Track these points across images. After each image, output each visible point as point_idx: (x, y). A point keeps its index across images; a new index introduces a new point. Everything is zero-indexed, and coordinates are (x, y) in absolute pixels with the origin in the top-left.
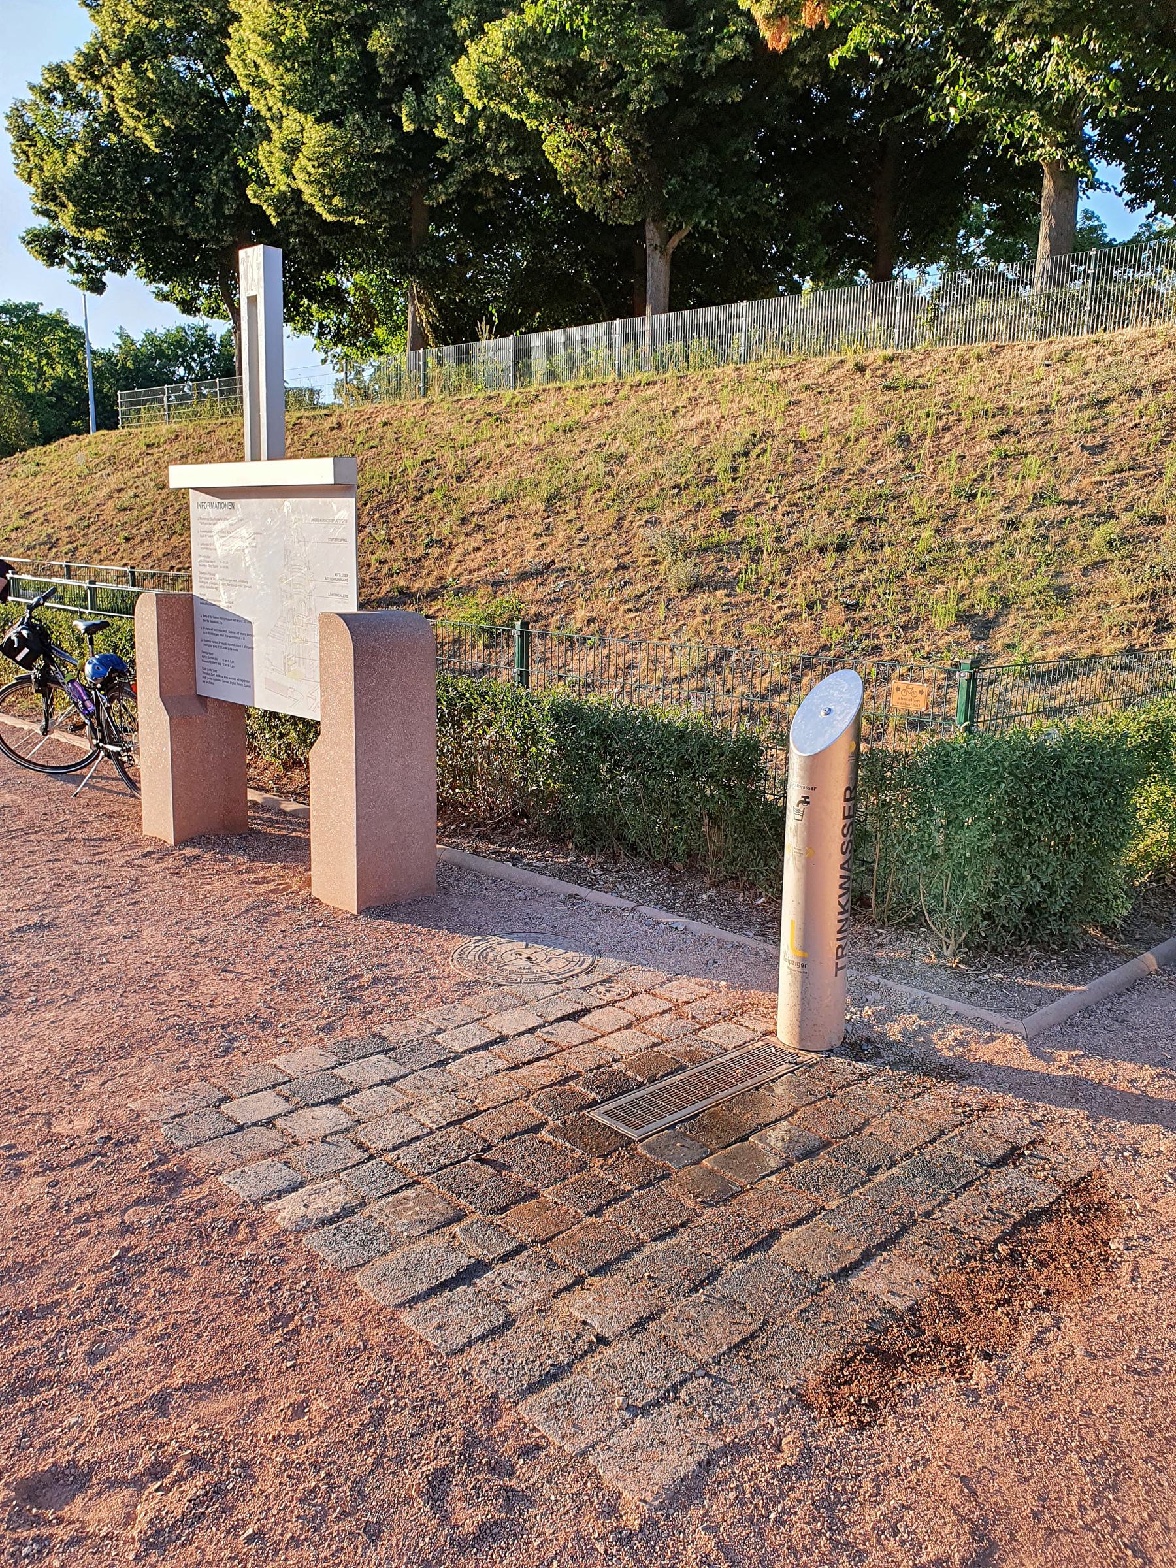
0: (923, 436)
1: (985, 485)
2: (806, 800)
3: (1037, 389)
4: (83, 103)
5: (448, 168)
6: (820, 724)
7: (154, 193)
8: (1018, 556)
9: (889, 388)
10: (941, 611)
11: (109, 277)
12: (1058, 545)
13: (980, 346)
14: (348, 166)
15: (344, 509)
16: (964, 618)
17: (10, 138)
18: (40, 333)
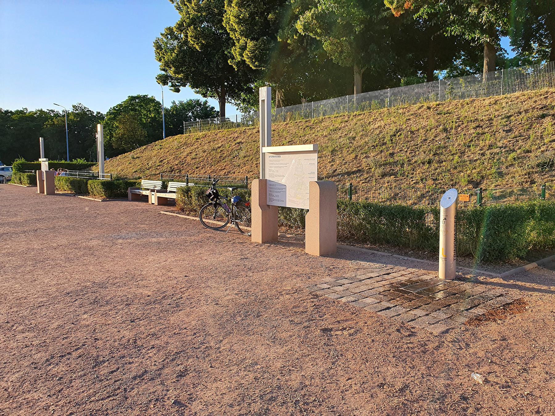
0: (452, 128)
1: (473, 143)
2: (445, 219)
3: (487, 113)
4: (177, 38)
5: (292, 52)
6: (448, 202)
7: (198, 62)
8: (485, 163)
9: (439, 114)
10: (463, 180)
11: (181, 88)
12: (497, 160)
13: (467, 100)
14: (260, 52)
15: (315, 156)
16: (470, 182)
17: (154, 49)
18: (146, 105)
